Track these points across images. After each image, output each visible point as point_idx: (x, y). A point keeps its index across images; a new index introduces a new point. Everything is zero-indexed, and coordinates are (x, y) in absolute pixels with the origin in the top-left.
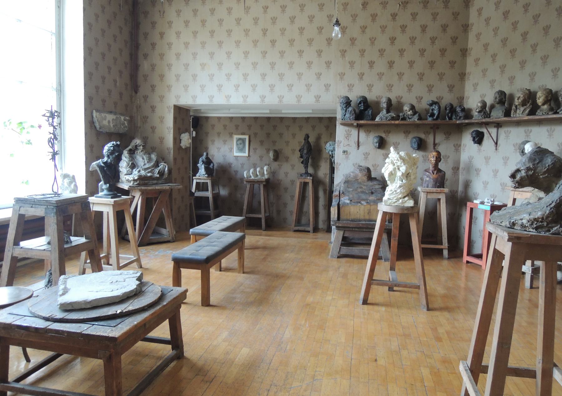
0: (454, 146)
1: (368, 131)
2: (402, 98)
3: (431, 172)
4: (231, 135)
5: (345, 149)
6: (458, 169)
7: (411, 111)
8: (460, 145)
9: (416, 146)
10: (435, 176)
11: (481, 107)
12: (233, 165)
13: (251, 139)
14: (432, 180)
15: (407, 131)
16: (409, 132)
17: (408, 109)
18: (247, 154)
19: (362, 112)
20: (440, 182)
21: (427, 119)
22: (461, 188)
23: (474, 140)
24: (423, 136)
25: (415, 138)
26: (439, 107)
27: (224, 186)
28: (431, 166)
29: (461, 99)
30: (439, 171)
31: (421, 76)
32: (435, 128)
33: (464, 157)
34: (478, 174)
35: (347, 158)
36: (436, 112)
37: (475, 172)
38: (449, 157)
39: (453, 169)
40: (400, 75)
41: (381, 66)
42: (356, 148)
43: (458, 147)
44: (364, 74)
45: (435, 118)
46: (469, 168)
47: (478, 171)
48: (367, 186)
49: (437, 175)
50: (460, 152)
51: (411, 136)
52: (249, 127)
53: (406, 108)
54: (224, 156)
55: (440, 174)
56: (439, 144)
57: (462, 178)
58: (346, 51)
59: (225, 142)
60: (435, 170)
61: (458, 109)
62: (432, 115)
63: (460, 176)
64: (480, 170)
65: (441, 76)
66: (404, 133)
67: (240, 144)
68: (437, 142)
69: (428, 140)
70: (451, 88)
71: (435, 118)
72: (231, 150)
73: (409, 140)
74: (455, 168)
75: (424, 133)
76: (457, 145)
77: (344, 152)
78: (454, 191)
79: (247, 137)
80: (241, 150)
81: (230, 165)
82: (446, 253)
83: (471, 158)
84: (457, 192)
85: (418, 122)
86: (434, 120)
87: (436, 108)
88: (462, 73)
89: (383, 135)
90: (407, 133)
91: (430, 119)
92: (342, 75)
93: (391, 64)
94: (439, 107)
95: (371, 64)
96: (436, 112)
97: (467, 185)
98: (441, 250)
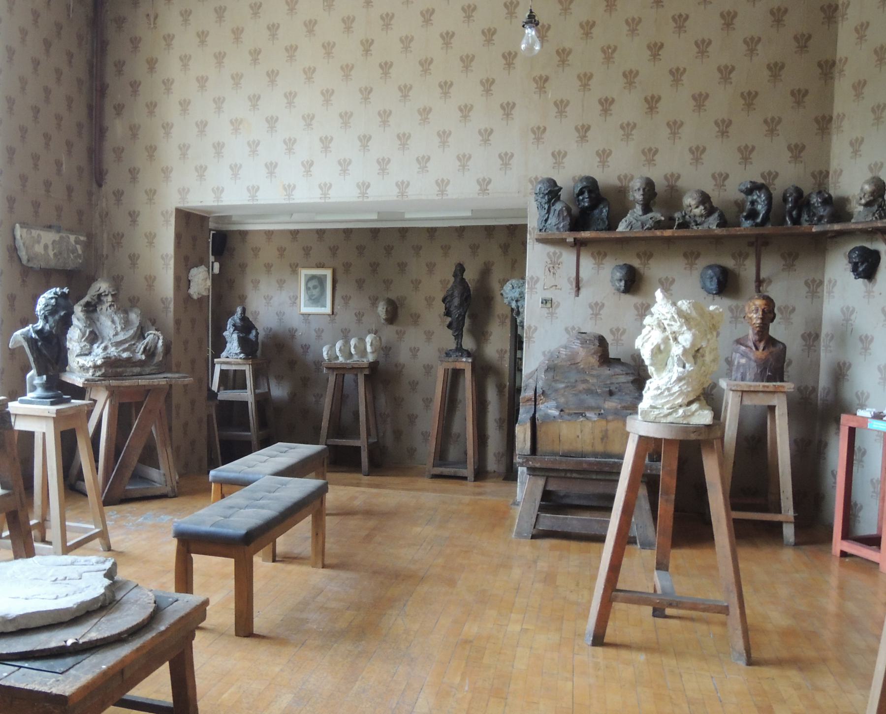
0: (806, 283)
1: (599, 253)
2: (679, 177)
3: (751, 344)
4: (294, 269)
5: (548, 295)
6: (817, 336)
7: (701, 207)
8: (821, 283)
9: (713, 285)
10: (760, 354)
11: (872, 193)
12: (298, 334)
13: (338, 277)
14: (753, 364)
15: (692, 253)
16: (698, 256)
17: (693, 203)
18: (328, 310)
19: (586, 213)
20: (774, 367)
21: (739, 225)
22: (824, 382)
23: (855, 270)
24: (729, 263)
25: (710, 267)
26: (769, 198)
27: (279, 378)
28: (751, 332)
29: (822, 177)
30: (772, 342)
31: (724, 127)
32: (759, 245)
33: (832, 308)
34: (866, 349)
35: (552, 314)
36: (761, 208)
37: (860, 345)
38: (794, 309)
39: (803, 337)
40: (675, 127)
41: (629, 107)
42: (573, 291)
43: (815, 287)
44: (589, 128)
45: (759, 220)
46: (844, 334)
47: (866, 341)
48: (598, 377)
49: (766, 353)
50: (821, 298)
51: (702, 263)
52: (334, 250)
53: (689, 201)
54: (280, 314)
55: (772, 349)
56: (770, 282)
57: (826, 358)
58: (547, 79)
59: (281, 283)
60: (760, 341)
61: (815, 200)
62: (752, 214)
63: (822, 354)
64: (872, 340)
65: (772, 126)
66: (685, 255)
67: (315, 287)
68: (763, 275)
69: (743, 273)
70: (797, 151)
71: (759, 220)
72: (295, 300)
73: (696, 274)
74: (810, 335)
75: (734, 256)
76: (814, 281)
77: (545, 302)
78: (806, 388)
79: (328, 273)
80: (316, 300)
81: (292, 333)
82: (789, 531)
83: (847, 313)
84: (815, 390)
85: (719, 231)
86: (757, 225)
87: (760, 198)
88: (824, 117)
89: (636, 263)
90: (691, 256)
91: (747, 224)
92: (539, 133)
93: (652, 103)
94: (769, 198)
95: (606, 104)
96: (761, 208)
97: (840, 374)
98: (779, 525)
